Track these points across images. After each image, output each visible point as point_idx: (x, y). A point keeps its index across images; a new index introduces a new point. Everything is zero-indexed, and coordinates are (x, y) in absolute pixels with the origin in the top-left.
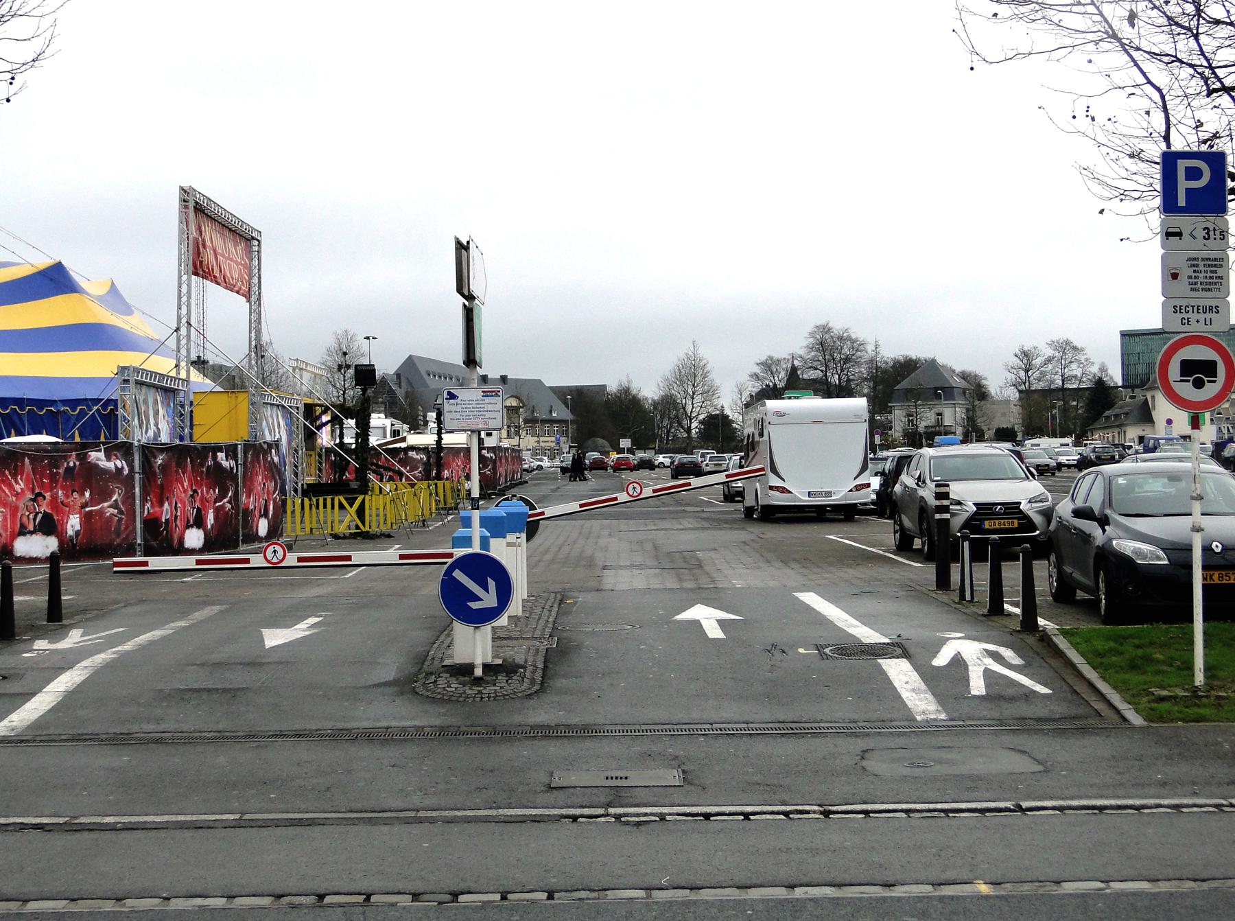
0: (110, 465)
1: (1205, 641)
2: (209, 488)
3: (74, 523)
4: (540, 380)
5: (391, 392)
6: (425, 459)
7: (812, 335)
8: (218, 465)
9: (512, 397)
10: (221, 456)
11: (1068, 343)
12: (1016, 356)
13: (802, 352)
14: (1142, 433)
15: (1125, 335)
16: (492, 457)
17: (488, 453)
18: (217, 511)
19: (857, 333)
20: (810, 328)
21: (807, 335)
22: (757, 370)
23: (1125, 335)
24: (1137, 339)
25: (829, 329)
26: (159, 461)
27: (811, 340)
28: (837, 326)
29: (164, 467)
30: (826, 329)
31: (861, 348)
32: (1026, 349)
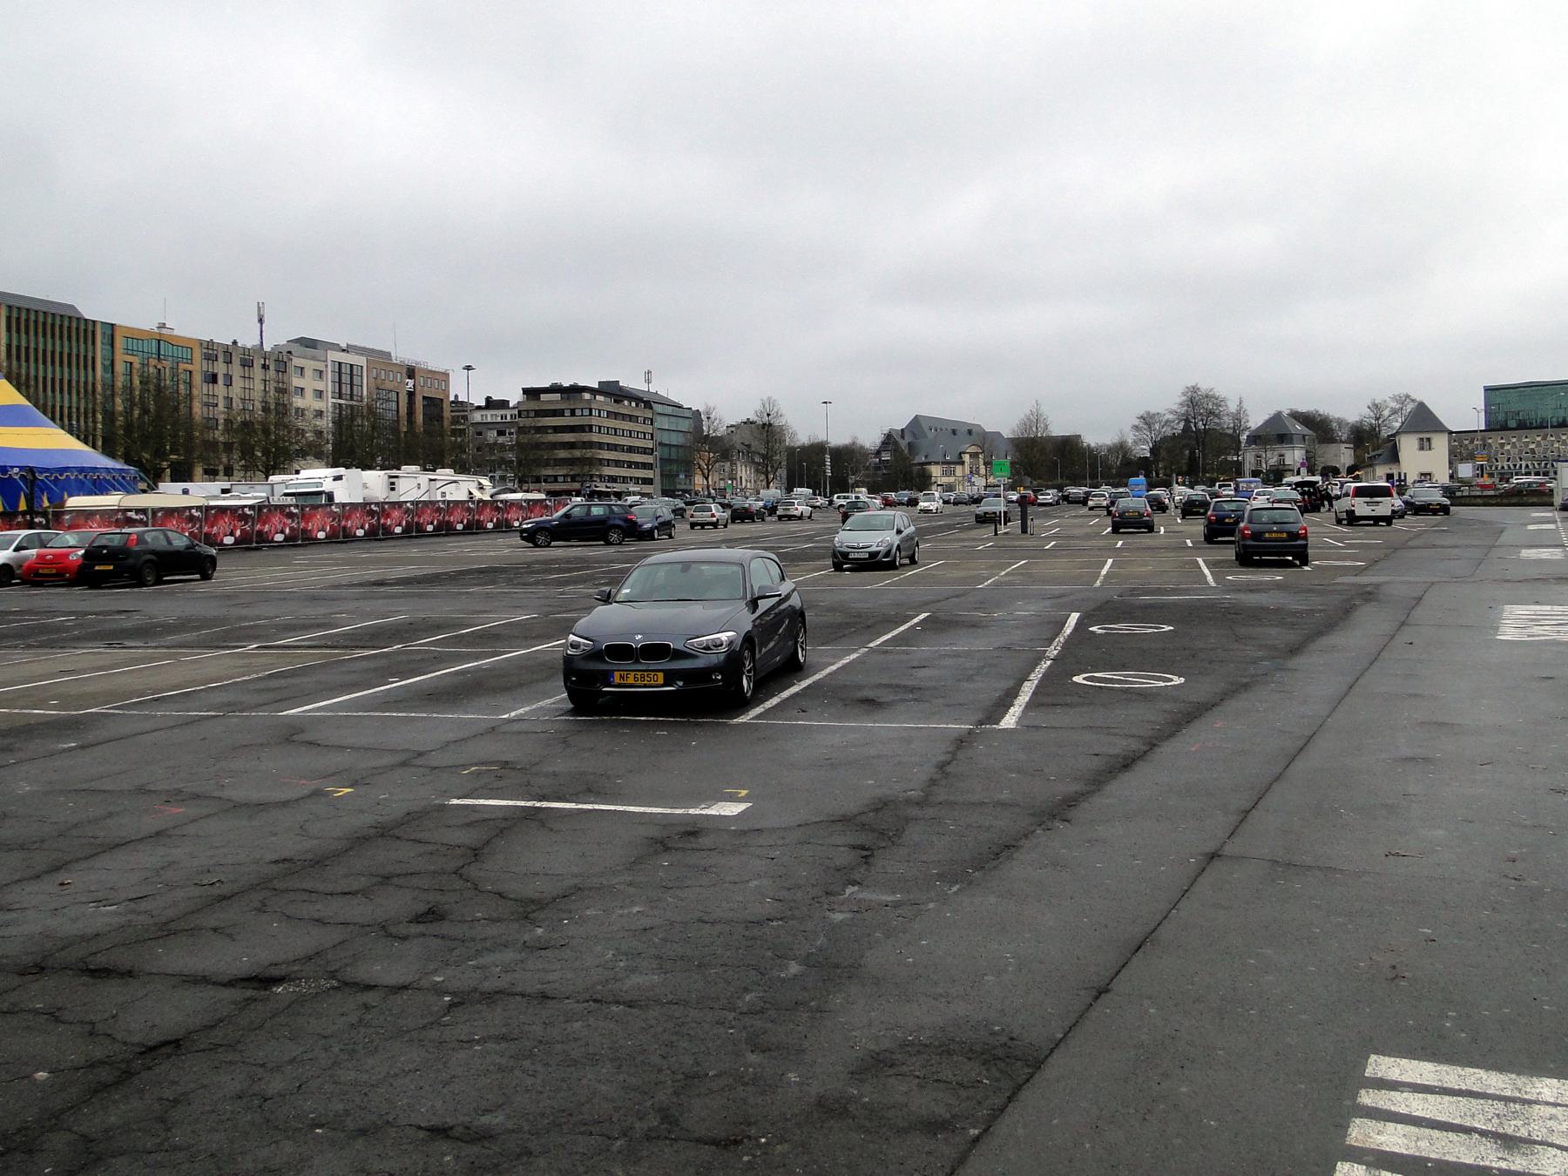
0: (137, 517)
1: (13, 543)
2: (186, 524)
3: (287, 531)
4: (999, 433)
5: (896, 443)
6: (44, 522)
7: (1184, 394)
8: (371, 509)
9: (974, 445)
10: (193, 511)
11: (1408, 396)
12: (1369, 407)
13: (1175, 407)
14: (1390, 472)
15: (1487, 389)
16: (142, 519)
17: (197, 511)
18: (331, 526)
19: (1220, 392)
20: (1181, 389)
21: (1180, 394)
22: (1137, 422)
23: (1487, 389)
24: (1497, 393)
25: (1198, 389)
26: (348, 508)
27: (1184, 398)
28: (1204, 386)
29: (453, 507)
30: (1195, 389)
31: (1223, 403)
32: (1376, 402)
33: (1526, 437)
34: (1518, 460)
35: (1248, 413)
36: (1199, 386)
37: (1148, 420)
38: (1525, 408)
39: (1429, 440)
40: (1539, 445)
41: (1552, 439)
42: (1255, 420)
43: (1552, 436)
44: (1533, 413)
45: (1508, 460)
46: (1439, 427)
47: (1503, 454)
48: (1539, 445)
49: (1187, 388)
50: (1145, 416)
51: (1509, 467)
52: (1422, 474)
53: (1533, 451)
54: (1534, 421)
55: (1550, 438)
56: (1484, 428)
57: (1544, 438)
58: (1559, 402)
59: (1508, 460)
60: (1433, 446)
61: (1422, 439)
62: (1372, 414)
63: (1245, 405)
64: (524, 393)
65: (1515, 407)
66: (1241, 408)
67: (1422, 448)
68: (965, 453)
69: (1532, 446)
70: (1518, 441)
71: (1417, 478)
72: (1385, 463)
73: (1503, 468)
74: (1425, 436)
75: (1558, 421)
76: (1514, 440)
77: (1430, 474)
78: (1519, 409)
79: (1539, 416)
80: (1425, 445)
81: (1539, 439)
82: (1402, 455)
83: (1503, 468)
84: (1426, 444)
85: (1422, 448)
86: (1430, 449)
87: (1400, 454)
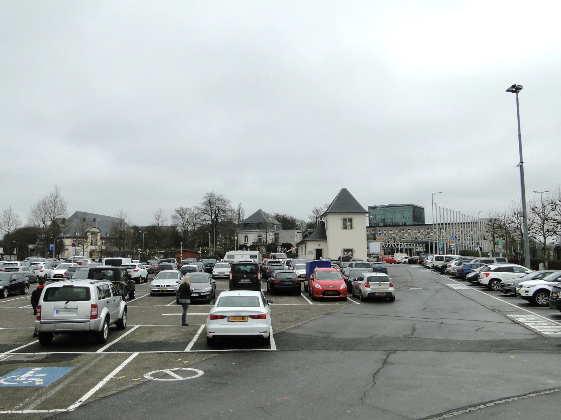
7: (206, 197)
22: (174, 213)
33: (391, 231)
34: (387, 243)
35: (245, 211)
36: (214, 193)
37: (181, 212)
38: (388, 217)
39: (350, 220)
40: (397, 234)
41: (391, 232)
42: (247, 214)
43: (403, 230)
44: (391, 220)
45: (394, 242)
46: (360, 211)
47: (391, 239)
48: (397, 234)
49: (208, 194)
50: (179, 209)
51: (394, 245)
52: (345, 251)
53: (394, 238)
54: (391, 224)
55: (402, 232)
56: (368, 226)
57: (400, 231)
58: (402, 215)
59: (394, 242)
60: (354, 225)
61: (345, 220)
62: (314, 215)
63: (243, 206)
64: (398, 253)
65: (383, 217)
66: (240, 208)
67: (345, 228)
68: (88, 232)
69: (394, 235)
70: (399, 232)
71: (342, 255)
72: (313, 240)
73: (392, 246)
74: (347, 217)
75: (402, 224)
76: (385, 232)
77: (351, 250)
78: (384, 218)
79: (394, 221)
80: (347, 224)
81: (397, 232)
82: (329, 233)
83: (392, 246)
84: (348, 224)
85: (345, 228)
86: (351, 228)
87: (327, 232)
